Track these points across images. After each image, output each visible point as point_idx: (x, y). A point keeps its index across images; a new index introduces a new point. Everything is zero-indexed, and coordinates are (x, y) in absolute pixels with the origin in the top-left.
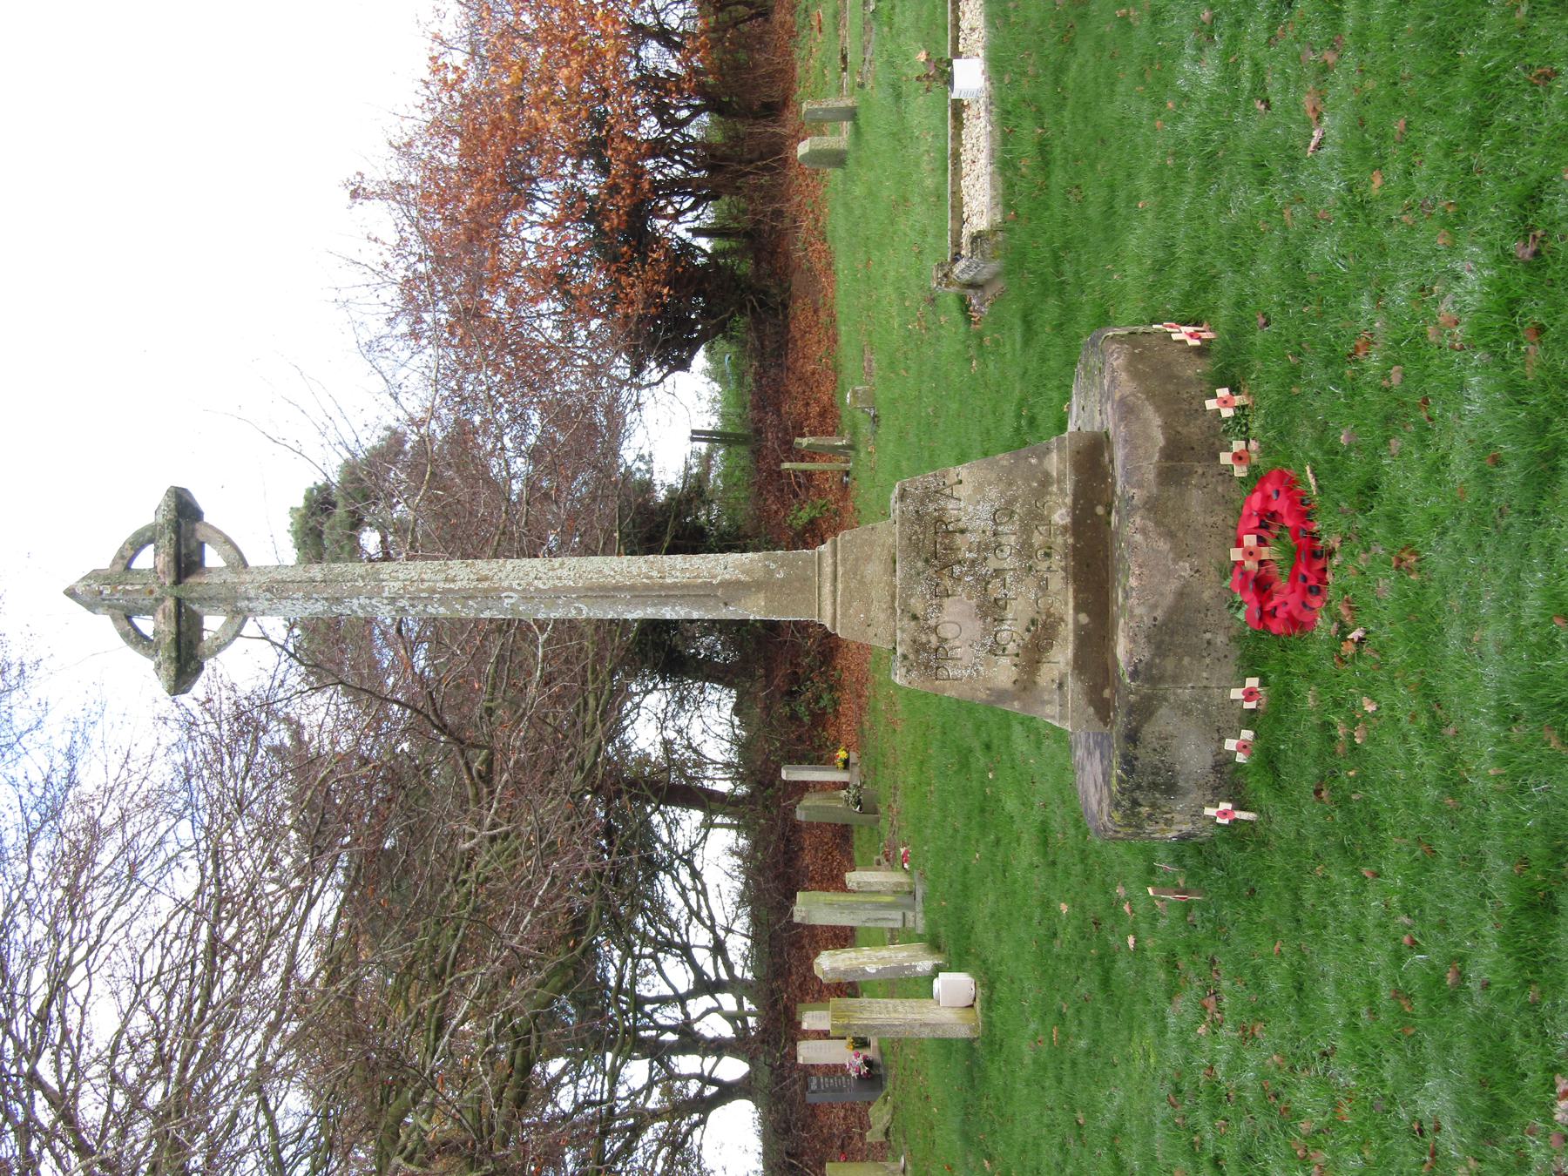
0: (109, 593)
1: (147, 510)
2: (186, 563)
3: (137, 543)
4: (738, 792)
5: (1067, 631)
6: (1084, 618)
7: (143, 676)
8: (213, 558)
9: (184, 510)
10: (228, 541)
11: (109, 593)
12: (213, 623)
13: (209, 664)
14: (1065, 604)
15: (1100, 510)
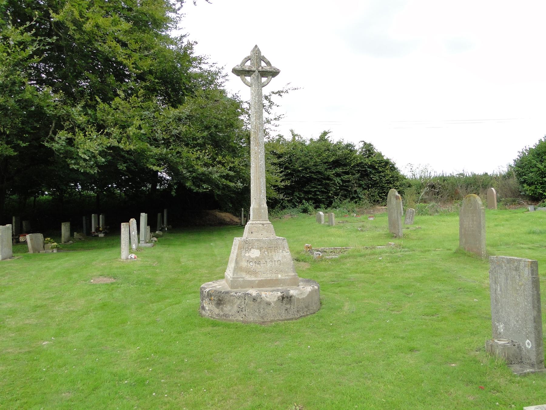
0: (257, 55)
1: (275, 64)
2: (264, 74)
3: (268, 63)
4: (32, 198)
5: (253, 278)
6: (257, 282)
7: (237, 62)
8: (264, 80)
9: (274, 73)
10: (244, 82)
11: (257, 55)
12: (248, 79)
13: (239, 78)
14: (261, 277)
15: (281, 285)
